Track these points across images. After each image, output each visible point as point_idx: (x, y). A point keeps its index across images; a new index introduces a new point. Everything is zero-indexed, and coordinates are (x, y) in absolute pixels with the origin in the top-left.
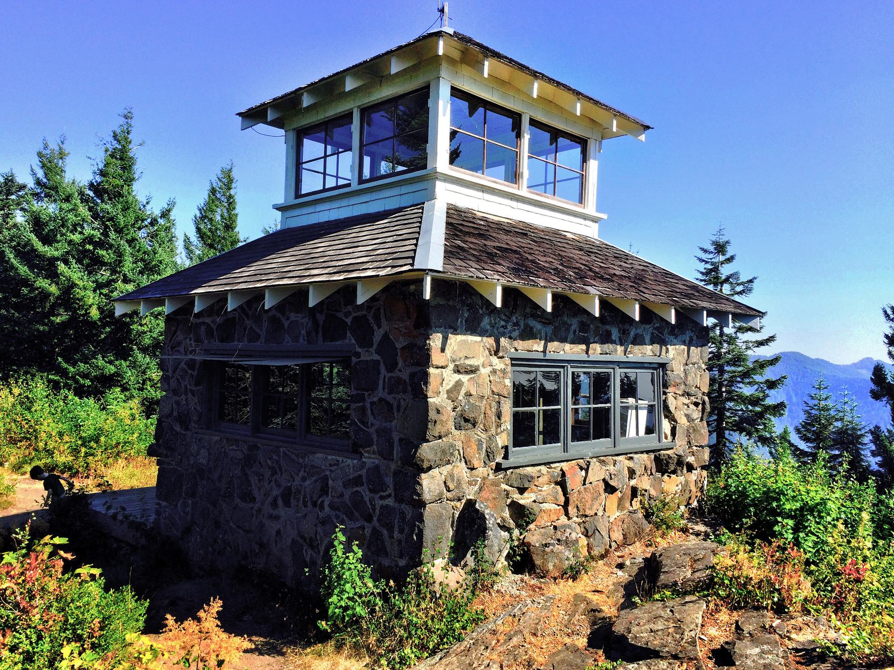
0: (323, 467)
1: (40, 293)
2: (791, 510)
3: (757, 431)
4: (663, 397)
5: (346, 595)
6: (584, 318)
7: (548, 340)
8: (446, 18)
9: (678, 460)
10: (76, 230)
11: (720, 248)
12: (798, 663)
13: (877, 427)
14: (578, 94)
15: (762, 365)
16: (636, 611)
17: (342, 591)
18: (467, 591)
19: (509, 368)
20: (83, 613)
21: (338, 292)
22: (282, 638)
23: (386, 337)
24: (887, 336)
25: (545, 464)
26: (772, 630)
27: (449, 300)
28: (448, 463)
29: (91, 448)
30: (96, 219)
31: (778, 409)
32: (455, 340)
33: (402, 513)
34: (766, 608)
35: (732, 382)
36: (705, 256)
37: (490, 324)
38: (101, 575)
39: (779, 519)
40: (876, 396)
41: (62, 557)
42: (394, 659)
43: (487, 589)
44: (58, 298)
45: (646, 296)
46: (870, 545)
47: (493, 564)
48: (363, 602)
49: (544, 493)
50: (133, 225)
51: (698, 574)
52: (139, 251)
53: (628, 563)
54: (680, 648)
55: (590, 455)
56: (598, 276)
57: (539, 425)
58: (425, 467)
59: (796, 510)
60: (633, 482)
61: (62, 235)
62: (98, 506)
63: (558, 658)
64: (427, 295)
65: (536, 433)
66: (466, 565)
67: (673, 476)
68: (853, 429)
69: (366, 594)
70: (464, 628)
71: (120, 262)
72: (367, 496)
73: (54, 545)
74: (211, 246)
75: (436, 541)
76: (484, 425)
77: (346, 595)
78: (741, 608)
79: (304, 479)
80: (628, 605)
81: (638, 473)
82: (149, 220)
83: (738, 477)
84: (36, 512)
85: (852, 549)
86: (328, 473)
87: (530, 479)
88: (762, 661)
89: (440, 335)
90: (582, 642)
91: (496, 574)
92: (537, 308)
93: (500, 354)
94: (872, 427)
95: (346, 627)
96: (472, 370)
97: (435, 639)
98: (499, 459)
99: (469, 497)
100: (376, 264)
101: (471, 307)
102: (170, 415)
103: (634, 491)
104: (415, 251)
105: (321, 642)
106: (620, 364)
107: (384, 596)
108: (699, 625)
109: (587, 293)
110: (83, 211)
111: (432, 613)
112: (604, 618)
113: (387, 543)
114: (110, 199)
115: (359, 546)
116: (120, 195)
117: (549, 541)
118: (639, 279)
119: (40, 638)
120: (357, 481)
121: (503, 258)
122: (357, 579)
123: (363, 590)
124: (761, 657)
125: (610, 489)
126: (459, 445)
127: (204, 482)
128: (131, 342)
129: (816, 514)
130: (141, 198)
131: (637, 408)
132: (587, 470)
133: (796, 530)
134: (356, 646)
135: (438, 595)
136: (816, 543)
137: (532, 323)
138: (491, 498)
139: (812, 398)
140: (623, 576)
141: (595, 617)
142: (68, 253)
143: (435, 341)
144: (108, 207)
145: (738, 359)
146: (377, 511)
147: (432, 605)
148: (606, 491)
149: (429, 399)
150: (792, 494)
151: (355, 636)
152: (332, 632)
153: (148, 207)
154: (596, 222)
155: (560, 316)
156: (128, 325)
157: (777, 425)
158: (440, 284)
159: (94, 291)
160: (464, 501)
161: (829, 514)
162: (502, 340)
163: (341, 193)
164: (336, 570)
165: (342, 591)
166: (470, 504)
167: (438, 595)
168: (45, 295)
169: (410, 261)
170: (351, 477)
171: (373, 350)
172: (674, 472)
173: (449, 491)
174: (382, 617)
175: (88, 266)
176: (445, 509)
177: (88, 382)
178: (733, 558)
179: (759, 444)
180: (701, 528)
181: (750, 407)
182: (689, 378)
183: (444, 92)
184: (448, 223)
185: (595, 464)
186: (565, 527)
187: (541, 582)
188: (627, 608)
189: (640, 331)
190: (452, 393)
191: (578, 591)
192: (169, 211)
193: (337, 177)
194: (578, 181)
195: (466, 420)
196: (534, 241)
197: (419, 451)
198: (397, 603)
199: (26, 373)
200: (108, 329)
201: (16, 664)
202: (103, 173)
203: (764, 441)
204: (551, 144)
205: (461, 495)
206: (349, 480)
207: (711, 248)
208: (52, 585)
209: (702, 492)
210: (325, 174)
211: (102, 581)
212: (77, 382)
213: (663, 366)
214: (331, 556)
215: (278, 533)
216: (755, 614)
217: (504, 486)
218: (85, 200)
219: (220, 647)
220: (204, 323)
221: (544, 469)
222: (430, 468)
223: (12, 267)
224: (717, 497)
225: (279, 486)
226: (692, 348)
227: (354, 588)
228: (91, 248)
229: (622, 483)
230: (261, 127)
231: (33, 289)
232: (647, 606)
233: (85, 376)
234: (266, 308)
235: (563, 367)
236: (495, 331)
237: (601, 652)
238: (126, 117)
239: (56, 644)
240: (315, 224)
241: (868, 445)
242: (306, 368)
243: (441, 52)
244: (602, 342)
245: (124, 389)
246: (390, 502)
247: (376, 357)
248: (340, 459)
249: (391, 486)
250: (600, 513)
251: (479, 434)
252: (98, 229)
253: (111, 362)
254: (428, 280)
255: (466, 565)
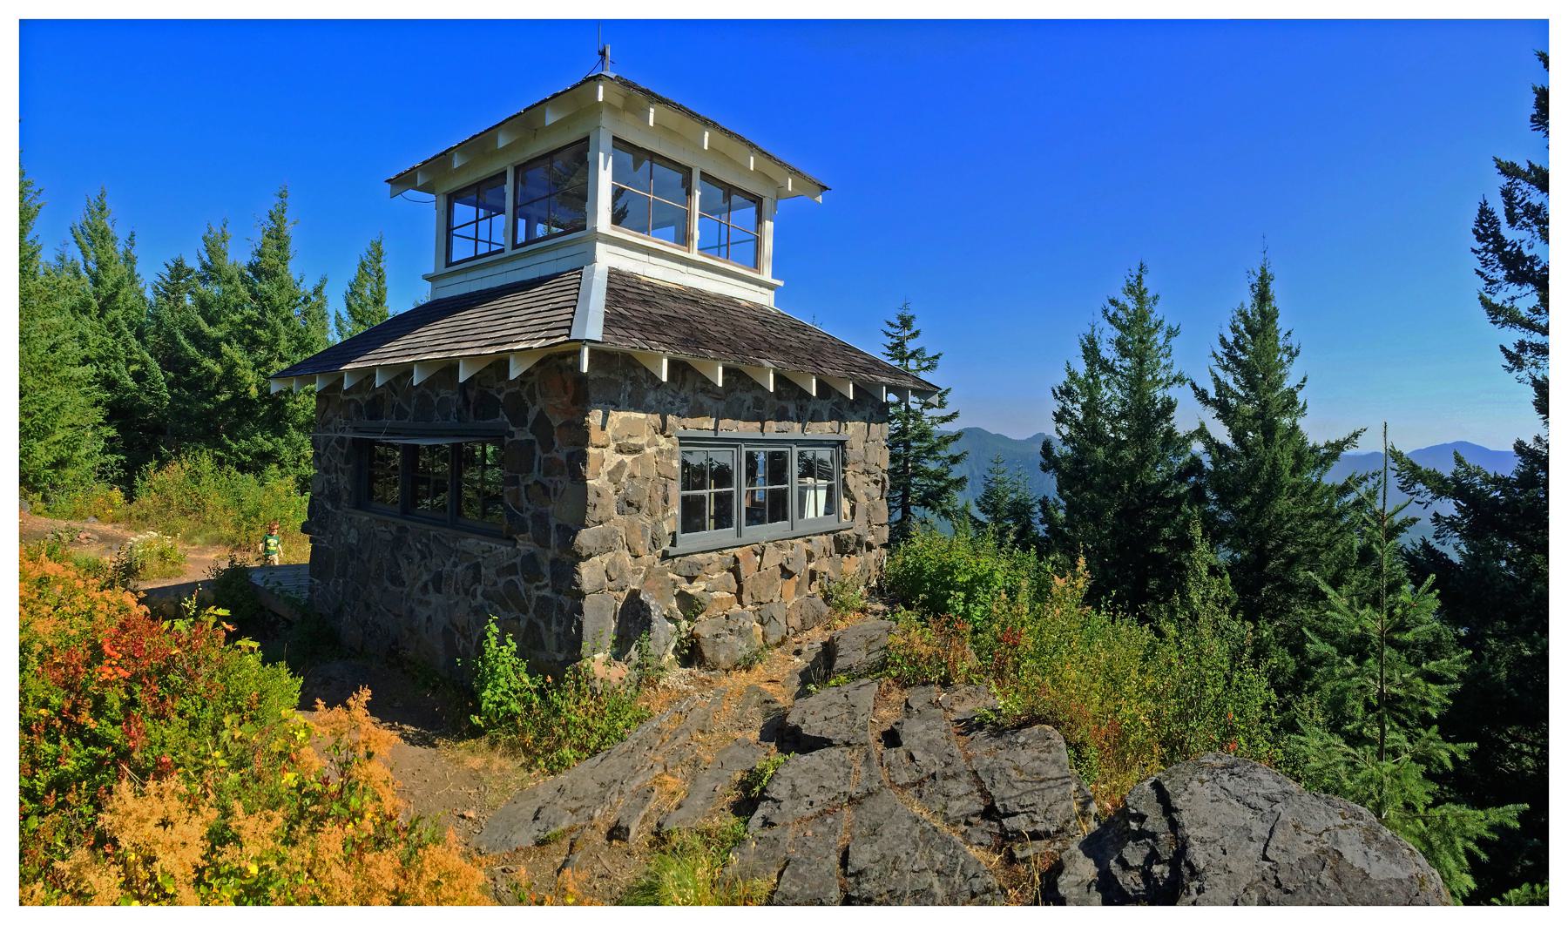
0: (476, 554)
1: (206, 373)
2: (963, 583)
3: (941, 505)
4: (842, 476)
5: (500, 690)
6: (759, 394)
7: (719, 417)
8: (607, 61)
9: (858, 540)
10: (237, 311)
11: (906, 323)
12: (958, 734)
13: (1045, 498)
14: (751, 145)
15: (946, 440)
16: (811, 699)
17: (496, 686)
18: (631, 688)
19: (677, 448)
20: (242, 685)
21: (490, 366)
22: (433, 730)
23: (541, 413)
24: (1055, 414)
25: (716, 550)
26: (938, 705)
27: (609, 374)
28: (610, 550)
29: (252, 522)
30: (255, 300)
31: (960, 483)
32: (616, 417)
33: (561, 605)
34: (934, 683)
35: (917, 458)
36: (892, 331)
37: (656, 400)
38: (259, 649)
39: (952, 592)
40: (1045, 469)
41: (224, 629)
42: (552, 759)
43: (653, 684)
44: (222, 377)
45: (824, 369)
46: (1027, 610)
47: (660, 658)
48: (518, 699)
49: (716, 582)
50: (288, 304)
51: (872, 656)
52: (293, 329)
53: (805, 649)
54: (851, 735)
55: (766, 539)
56: (774, 349)
57: (710, 508)
58: (584, 554)
59: (967, 582)
60: (811, 566)
61: (225, 316)
62: (257, 579)
63: (727, 755)
64: (585, 369)
65: (707, 517)
66: (630, 659)
67: (853, 557)
68: (1026, 499)
69: (521, 690)
70: (627, 727)
71: (276, 340)
72: (522, 586)
73: (217, 616)
74: (361, 322)
75: (598, 635)
76: (649, 510)
77: (500, 690)
78: (911, 686)
79: (455, 565)
80: (803, 693)
81: (817, 556)
82: (303, 298)
83: (916, 554)
84: (201, 582)
85: (1013, 616)
86: (480, 560)
87: (700, 567)
88: (926, 738)
89: (600, 412)
90: (754, 735)
91: (662, 669)
92: (708, 384)
93: (667, 433)
94: (1041, 497)
95: (500, 723)
96: (636, 450)
97: (596, 738)
98: (666, 547)
99: (632, 587)
100: (529, 336)
101: (634, 381)
102: (320, 494)
103: (813, 575)
104: (572, 320)
105: (475, 737)
106: (797, 442)
107: (541, 692)
108: (872, 709)
109: (761, 366)
110: (243, 291)
111: (592, 710)
112: (778, 709)
113: (545, 637)
114: (267, 279)
115: (513, 639)
116: (276, 274)
117: (721, 631)
118: (818, 352)
119: (204, 705)
120: (512, 569)
121: (667, 326)
122: (512, 674)
123: (519, 685)
124: (926, 734)
125: (787, 573)
126: (622, 531)
127: (355, 563)
128: (287, 419)
129: (984, 584)
130: (295, 277)
131: (815, 489)
132: (762, 556)
133: (966, 601)
134: (511, 745)
135: (599, 692)
136: (984, 612)
137: (701, 398)
138: (656, 587)
139: (991, 472)
140: (800, 663)
141: (769, 708)
142: (230, 333)
143: (595, 418)
144: (265, 286)
145: (923, 436)
146: (533, 603)
147: (592, 702)
148: (782, 576)
149: (588, 482)
150: (964, 567)
151: (510, 733)
152: (486, 727)
153: (301, 285)
154: (772, 289)
155: (732, 391)
156: (283, 403)
157: (959, 499)
158: (600, 356)
159: (254, 370)
160: (627, 591)
161: (996, 584)
162: (669, 417)
163: (494, 258)
164: (490, 664)
165: (496, 686)
166: (634, 594)
167: (599, 692)
168: (210, 375)
169: (566, 331)
170: (505, 565)
171: (527, 429)
172: (854, 552)
173: (611, 580)
174: (539, 714)
175: (248, 345)
176: (607, 600)
177: (248, 459)
178: (905, 637)
179: (942, 517)
180: (880, 607)
181: (935, 482)
182: (869, 456)
183: (606, 141)
184: (609, 289)
185: (770, 547)
186: (738, 615)
187: (710, 676)
188: (802, 696)
189: (817, 407)
190: (615, 474)
191: (751, 682)
192: (321, 288)
193: (490, 243)
194: (752, 244)
195: (630, 504)
196: (705, 309)
197: (578, 538)
198: (556, 700)
199: (196, 448)
200: (266, 407)
201: (183, 728)
202: (260, 254)
203: (946, 514)
204: (724, 202)
205: (623, 585)
206: (503, 568)
207: (898, 323)
208: (214, 655)
209: (881, 571)
210: (477, 240)
211: (260, 654)
212: (239, 458)
213: (842, 443)
214: (484, 648)
215: (429, 618)
216: (923, 689)
217: (671, 575)
218: (244, 280)
219: (369, 739)
220: (353, 400)
221: (715, 555)
222: (590, 556)
223: (183, 348)
224: (896, 575)
225: (428, 570)
226: (872, 425)
227: (509, 682)
228: (250, 328)
229: (801, 568)
230: (411, 194)
231: (200, 369)
232: (823, 692)
233: (246, 452)
234: (415, 384)
235: (736, 446)
236: (662, 408)
237: (773, 745)
238: (281, 196)
239: (218, 713)
240: (466, 294)
241: (1037, 514)
242: (456, 448)
243: (600, 99)
244: (779, 420)
245: (281, 466)
246: (547, 592)
247: (531, 437)
248: (493, 545)
249: (549, 576)
250: (776, 600)
251: (643, 519)
252: (257, 309)
253: (268, 439)
254: (586, 351)
255: (630, 659)
